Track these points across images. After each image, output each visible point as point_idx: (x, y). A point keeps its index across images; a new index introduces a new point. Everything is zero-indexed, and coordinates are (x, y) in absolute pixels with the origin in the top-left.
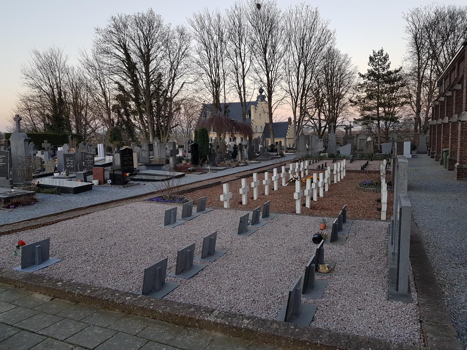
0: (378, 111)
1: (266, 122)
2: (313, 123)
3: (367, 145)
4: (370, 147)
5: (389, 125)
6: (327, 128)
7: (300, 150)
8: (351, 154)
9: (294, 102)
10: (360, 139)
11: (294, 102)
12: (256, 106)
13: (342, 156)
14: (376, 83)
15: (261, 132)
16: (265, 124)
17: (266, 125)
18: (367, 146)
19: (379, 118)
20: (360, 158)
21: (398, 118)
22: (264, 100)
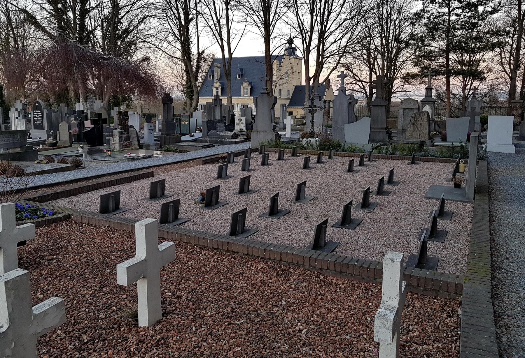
0: (448, 60)
1: (296, 85)
2: (361, 85)
3: (413, 121)
4: (419, 126)
5: (469, 92)
6: (375, 93)
7: (259, 129)
8: (371, 140)
9: (305, 44)
10: (405, 109)
11: (305, 44)
12: (280, 61)
13: (346, 148)
14: (446, 10)
15: (288, 98)
16: (294, 88)
17: (295, 88)
18: (414, 124)
19: (449, 73)
20: (389, 155)
21: (484, 73)
22: (294, 54)
